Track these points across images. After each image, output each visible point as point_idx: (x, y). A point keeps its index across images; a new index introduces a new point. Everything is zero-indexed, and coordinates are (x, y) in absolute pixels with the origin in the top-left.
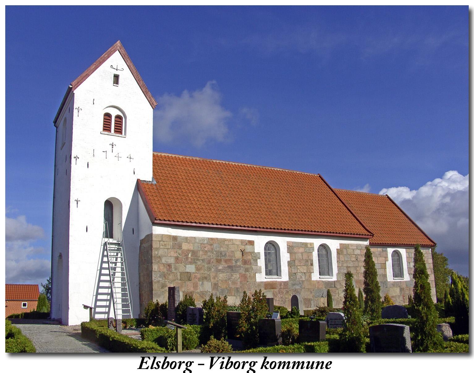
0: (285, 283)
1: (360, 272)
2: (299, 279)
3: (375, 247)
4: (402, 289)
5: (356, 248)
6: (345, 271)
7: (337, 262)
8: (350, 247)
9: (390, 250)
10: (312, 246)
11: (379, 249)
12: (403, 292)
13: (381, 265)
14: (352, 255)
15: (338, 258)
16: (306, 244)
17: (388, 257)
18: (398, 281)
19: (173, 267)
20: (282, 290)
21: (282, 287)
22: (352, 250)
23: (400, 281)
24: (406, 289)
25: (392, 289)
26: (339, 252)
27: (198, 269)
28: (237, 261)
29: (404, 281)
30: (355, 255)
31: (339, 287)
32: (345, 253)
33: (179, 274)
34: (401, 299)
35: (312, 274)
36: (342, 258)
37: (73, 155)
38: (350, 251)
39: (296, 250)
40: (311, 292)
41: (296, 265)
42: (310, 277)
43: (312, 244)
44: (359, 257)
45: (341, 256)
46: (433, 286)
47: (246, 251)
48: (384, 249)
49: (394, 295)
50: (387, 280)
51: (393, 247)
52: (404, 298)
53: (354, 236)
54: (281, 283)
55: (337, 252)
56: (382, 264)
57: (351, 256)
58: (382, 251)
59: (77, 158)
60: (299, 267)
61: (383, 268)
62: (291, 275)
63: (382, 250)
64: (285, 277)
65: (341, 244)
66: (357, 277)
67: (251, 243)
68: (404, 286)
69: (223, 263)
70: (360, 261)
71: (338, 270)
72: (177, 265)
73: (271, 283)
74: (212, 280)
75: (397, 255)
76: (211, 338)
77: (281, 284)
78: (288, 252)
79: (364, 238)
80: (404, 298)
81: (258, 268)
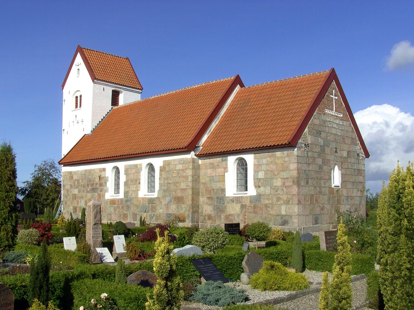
0: (122, 199)
1: (179, 188)
2: (130, 196)
3: (263, 151)
4: (243, 206)
5: (178, 163)
6: (165, 188)
7: (160, 179)
8: (173, 163)
9: (232, 160)
10: (141, 167)
11: (218, 159)
12: (244, 209)
13: (219, 177)
14: (174, 171)
15: (161, 175)
16: (136, 166)
17: (227, 168)
18: (240, 197)
19: (69, 191)
20: (119, 205)
21: (119, 203)
22: (174, 166)
23: (242, 196)
24: (249, 207)
25: (230, 206)
26: (162, 169)
27: (79, 191)
28: (97, 184)
29: (247, 197)
30: (177, 170)
31: (158, 203)
32: (167, 169)
33: (71, 195)
34: (240, 219)
35: (139, 191)
36: (164, 175)
37: (63, 129)
38: (172, 167)
39: (130, 171)
40: (138, 207)
41: (129, 184)
42: (137, 194)
43: (141, 165)
44: (180, 172)
45: (163, 173)
46: (294, 203)
47: (102, 176)
48: (224, 158)
49: (233, 213)
50: (225, 195)
51: (235, 155)
52: (246, 217)
53: (172, 152)
54: (118, 199)
55: (160, 170)
56: (220, 177)
57: (173, 172)
58: (221, 161)
59: (64, 130)
60: (131, 186)
61: (222, 181)
62: (126, 193)
63: (222, 159)
64: (121, 196)
65: (164, 161)
66: (176, 193)
67: (104, 170)
68: (248, 203)
69: (90, 186)
70: (181, 177)
71: (159, 187)
72: (71, 189)
73: (113, 200)
74: (85, 199)
75: (242, 164)
76: (257, 241)
77: (119, 200)
78: (125, 174)
79: (112, 159)
80: (246, 217)
81: (107, 189)
